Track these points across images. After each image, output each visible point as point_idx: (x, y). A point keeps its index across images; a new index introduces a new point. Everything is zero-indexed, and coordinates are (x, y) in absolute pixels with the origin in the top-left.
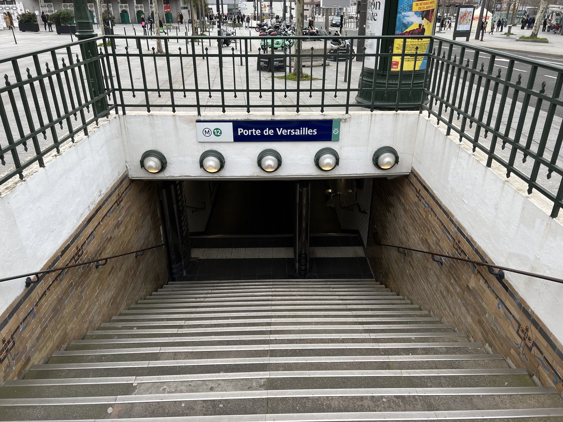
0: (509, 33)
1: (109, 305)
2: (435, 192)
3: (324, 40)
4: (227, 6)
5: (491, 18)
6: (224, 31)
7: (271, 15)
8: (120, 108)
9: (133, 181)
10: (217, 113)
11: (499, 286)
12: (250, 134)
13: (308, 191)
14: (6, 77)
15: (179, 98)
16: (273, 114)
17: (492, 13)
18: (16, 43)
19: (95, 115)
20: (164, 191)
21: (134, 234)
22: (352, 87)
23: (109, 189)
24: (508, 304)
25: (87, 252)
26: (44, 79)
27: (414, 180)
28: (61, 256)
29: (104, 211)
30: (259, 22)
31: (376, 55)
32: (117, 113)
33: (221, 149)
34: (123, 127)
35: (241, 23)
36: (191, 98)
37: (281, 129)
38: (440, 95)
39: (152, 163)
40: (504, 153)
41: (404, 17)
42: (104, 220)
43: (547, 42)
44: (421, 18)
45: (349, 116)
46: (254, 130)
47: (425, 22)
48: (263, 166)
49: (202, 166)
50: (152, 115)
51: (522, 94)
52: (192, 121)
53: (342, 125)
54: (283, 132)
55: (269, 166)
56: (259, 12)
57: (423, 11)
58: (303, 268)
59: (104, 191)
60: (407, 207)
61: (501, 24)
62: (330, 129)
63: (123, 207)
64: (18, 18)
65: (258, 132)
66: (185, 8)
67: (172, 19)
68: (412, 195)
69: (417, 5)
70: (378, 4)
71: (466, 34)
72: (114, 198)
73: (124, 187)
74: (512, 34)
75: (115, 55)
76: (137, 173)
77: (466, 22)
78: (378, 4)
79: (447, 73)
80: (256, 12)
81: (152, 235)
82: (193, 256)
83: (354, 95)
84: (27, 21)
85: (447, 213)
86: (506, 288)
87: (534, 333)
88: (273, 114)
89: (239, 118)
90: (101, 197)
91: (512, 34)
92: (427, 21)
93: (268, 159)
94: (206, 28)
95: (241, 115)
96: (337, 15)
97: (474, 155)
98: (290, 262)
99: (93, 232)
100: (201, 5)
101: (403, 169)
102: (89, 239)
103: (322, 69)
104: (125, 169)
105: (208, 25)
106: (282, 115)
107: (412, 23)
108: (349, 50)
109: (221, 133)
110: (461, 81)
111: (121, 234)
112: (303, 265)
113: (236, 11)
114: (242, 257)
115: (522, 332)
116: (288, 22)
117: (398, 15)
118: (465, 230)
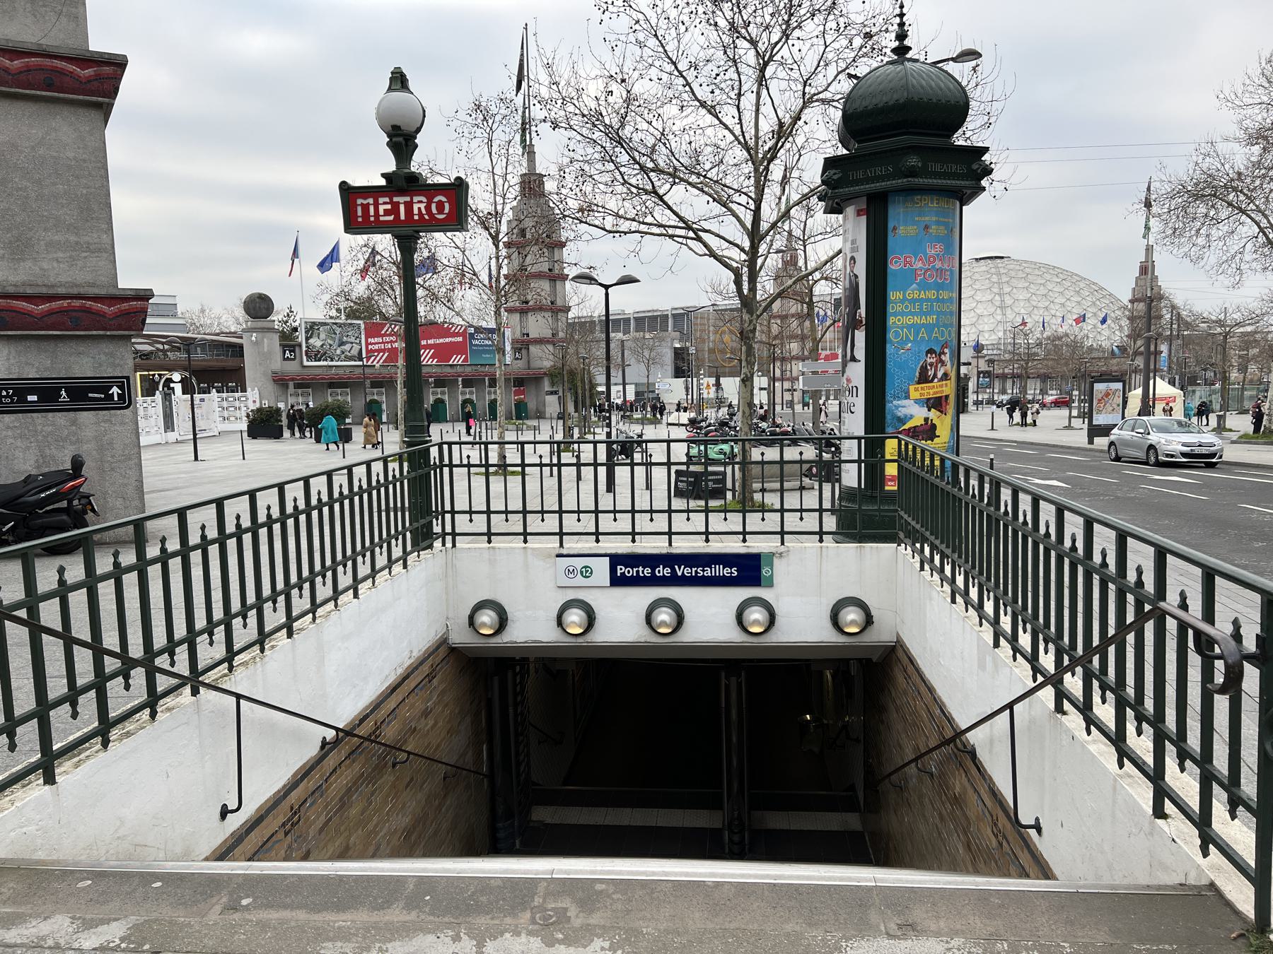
1: (400, 838)
2: (919, 662)
4: (633, 386)
5: (1180, 400)
6: (621, 432)
7: (720, 402)
8: (449, 538)
10: (587, 545)
11: (974, 771)
12: (635, 575)
13: (739, 685)
15: (570, 523)
16: (670, 544)
17: (1182, 390)
18: (244, 459)
20: (496, 679)
21: (444, 738)
23: (421, 653)
24: (982, 792)
25: (385, 735)
26: (40, 604)
27: (900, 653)
28: (359, 725)
29: (411, 683)
31: (859, 461)
32: (444, 544)
33: (591, 597)
34: (450, 565)
35: (658, 416)
36: (551, 523)
37: (683, 567)
39: (487, 618)
42: (411, 697)
44: (926, 409)
45: (786, 549)
46: (641, 569)
47: (933, 414)
48: (654, 625)
49: (560, 623)
50: (493, 548)
52: (549, 556)
53: (776, 561)
54: (685, 571)
55: (663, 624)
56: (695, 397)
57: (929, 399)
58: (736, 838)
59: (416, 654)
61: (1203, 410)
62: (758, 569)
63: (435, 687)
64: (248, 416)
65: (647, 572)
66: (551, 393)
67: (526, 413)
68: (900, 679)
69: (916, 390)
70: (855, 389)
72: (426, 669)
73: (438, 660)
74: (1230, 430)
75: (451, 466)
76: (461, 637)
77: (1111, 408)
78: (855, 389)
80: (690, 397)
81: (470, 754)
83: (830, 523)
84: (262, 421)
85: (931, 690)
88: (670, 544)
89: (620, 551)
90: (412, 661)
91: (1230, 430)
92: (938, 413)
93: (661, 612)
94: (589, 428)
95: (622, 546)
97: (943, 592)
98: (715, 834)
99: (395, 709)
100: (584, 390)
101: (881, 634)
102: (390, 718)
104: (445, 630)
105: (595, 422)
106: (683, 546)
107: (911, 417)
109: (591, 573)
111: (428, 731)
112: (736, 833)
113: (651, 396)
114: (626, 823)
117: (888, 406)
118: (945, 706)
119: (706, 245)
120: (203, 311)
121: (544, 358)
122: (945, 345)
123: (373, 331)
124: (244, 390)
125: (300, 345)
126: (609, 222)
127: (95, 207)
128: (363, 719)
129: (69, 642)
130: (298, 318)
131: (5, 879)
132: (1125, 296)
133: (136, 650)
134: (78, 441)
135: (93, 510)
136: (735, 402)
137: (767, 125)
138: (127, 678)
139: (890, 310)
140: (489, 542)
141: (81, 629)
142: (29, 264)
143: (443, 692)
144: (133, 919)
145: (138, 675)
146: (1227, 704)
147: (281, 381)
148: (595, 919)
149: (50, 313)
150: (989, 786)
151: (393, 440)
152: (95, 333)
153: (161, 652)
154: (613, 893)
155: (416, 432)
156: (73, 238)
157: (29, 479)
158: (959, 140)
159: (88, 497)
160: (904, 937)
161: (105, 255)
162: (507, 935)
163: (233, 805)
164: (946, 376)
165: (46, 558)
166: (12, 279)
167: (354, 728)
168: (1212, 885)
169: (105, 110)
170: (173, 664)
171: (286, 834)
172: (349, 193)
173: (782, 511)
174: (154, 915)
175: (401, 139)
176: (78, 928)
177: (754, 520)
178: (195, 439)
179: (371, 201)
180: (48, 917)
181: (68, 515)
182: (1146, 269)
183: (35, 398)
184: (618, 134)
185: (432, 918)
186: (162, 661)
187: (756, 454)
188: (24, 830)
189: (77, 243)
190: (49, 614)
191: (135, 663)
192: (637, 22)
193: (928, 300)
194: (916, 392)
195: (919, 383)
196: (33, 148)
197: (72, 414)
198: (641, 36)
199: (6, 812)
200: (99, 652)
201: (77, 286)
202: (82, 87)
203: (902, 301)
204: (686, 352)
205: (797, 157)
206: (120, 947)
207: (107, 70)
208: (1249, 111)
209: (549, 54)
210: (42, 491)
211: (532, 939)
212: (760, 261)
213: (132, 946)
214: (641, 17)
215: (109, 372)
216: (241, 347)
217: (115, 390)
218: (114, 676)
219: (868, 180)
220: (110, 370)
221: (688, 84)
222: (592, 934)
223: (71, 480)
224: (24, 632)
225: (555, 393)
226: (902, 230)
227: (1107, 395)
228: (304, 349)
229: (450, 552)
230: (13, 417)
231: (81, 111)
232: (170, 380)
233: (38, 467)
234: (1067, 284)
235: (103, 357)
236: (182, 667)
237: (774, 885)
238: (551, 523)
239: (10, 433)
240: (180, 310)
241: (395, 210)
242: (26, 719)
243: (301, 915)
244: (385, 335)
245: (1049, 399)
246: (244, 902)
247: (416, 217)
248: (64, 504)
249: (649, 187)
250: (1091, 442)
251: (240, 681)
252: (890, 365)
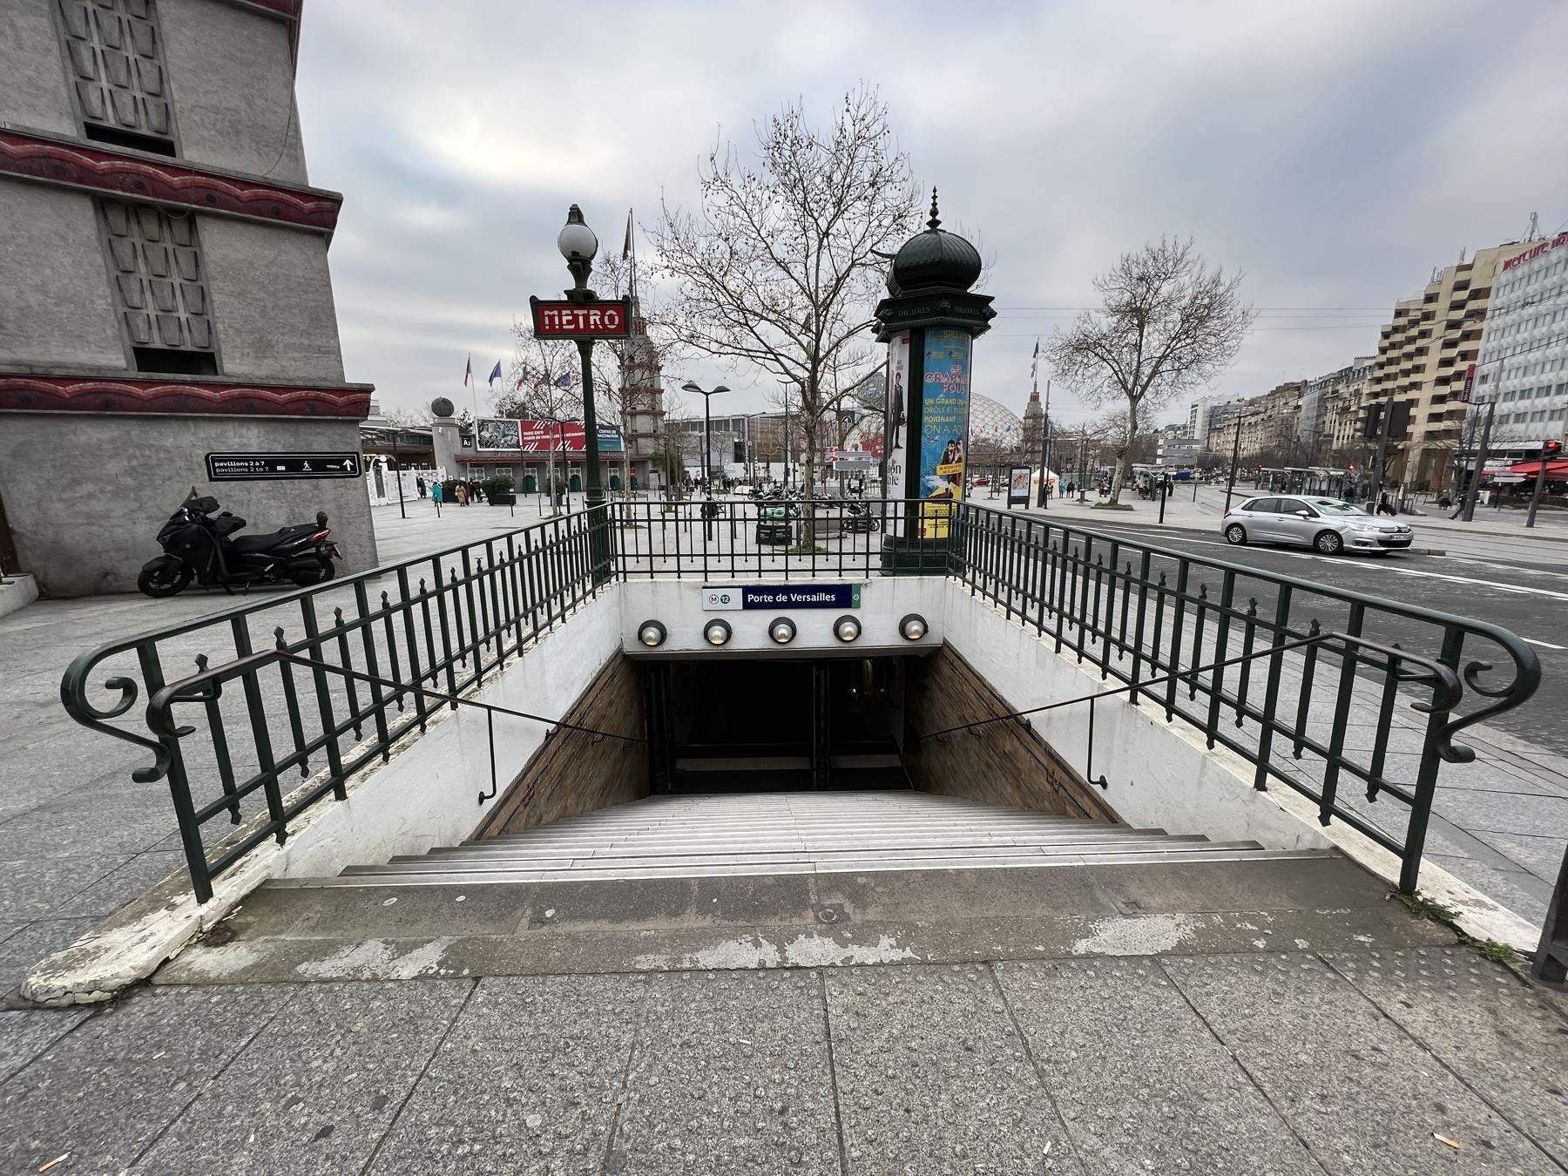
0: (1082, 499)
5: (1057, 481)
7: (768, 479)
8: (621, 575)
9: (625, 657)
10: (725, 579)
11: (1028, 738)
13: (826, 674)
15: (685, 563)
19: (593, 586)
24: (1037, 753)
27: (947, 652)
30: (752, 488)
36: (699, 563)
38: (994, 573)
39: (652, 633)
40: (1071, 634)
41: (928, 481)
43: (1132, 510)
47: (951, 486)
48: (775, 636)
51: (1080, 567)
55: (783, 636)
59: (603, 662)
60: (943, 685)
61: (1070, 488)
65: (770, 599)
66: (654, 472)
68: (946, 669)
71: (1025, 500)
72: (609, 671)
76: (632, 647)
82: (678, 767)
83: (876, 562)
85: (980, 679)
86: (1034, 738)
87: (1059, 774)
95: (752, 580)
96: (856, 479)
101: (934, 639)
103: (838, 541)
106: (796, 580)
107: (938, 487)
108: (868, 518)
110: (1016, 555)
115: (1050, 776)
116: (790, 486)
118: (996, 691)
119: (782, 365)
120: (399, 412)
121: (648, 447)
122: (959, 439)
123: (527, 427)
124: (434, 467)
125: (474, 436)
126: (714, 347)
127: (323, 317)
128: (572, 713)
129: (350, 676)
130: (471, 417)
131: (310, 902)
132: (1021, 416)
133: (406, 678)
134: (321, 502)
135: (337, 555)
137: (827, 276)
138: (400, 700)
139: (924, 412)
140: (652, 577)
141: (359, 664)
142: (270, 361)
143: (620, 689)
144: (446, 940)
145: (409, 697)
147: (461, 462)
148: (872, 914)
149: (291, 401)
150: (1045, 750)
151: (577, 502)
152: (329, 417)
153: (426, 677)
154: (876, 886)
155: (594, 495)
156: (306, 342)
157: (282, 531)
158: (972, 290)
159: (332, 545)
160: (1134, 916)
161: (333, 356)
162: (802, 937)
163: (488, 792)
164: (960, 460)
166: (257, 373)
167: (566, 721)
168: (1336, 849)
169: (326, 238)
170: (436, 686)
171: (525, 806)
172: (538, 306)
173: (840, 554)
174: (466, 934)
175: (579, 263)
176: (393, 955)
177: (821, 561)
178: (402, 502)
179: (556, 313)
180: (360, 944)
181: (318, 558)
182: (1035, 398)
183: (283, 468)
185: (726, 922)
186: (427, 685)
187: (820, 514)
188: (321, 844)
189: (310, 346)
190: (330, 652)
191: (405, 689)
192: (732, 198)
193: (949, 405)
194: (942, 470)
195: (943, 464)
196: (267, 266)
197: (314, 481)
198: (736, 209)
199: (304, 831)
200: (375, 681)
201: (311, 380)
202: (306, 217)
203: (933, 406)
205: (840, 306)
206: (439, 974)
207: (326, 204)
208: (1112, 294)
209: (672, 215)
210: (295, 541)
211: (826, 940)
212: (819, 375)
213: (452, 972)
214: (734, 195)
215: (343, 449)
216: (431, 437)
217: (348, 463)
218: (390, 700)
219: (908, 318)
220: (342, 447)
221: (768, 247)
222: (877, 931)
223: (317, 532)
224: (309, 671)
225: (656, 472)
226: (934, 354)
227: (1020, 477)
228: (478, 439)
229: (622, 585)
230: (266, 482)
231: (306, 238)
232: (378, 461)
233: (290, 522)
234: (986, 406)
235: (337, 437)
236: (443, 689)
237: (1005, 869)
238: (672, 563)
239: (264, 495)
240: (381, 411)
241: (575, 321)
242: (316, 746)
243: (605, 926)
244: (536, 430)
245: (975, 480)
246: (549, 914)
247: (592, 327)
248: (313, 550)
249: (742, 321)
250: (1009, 507)
251: (487, 695)
252: (924, 451)
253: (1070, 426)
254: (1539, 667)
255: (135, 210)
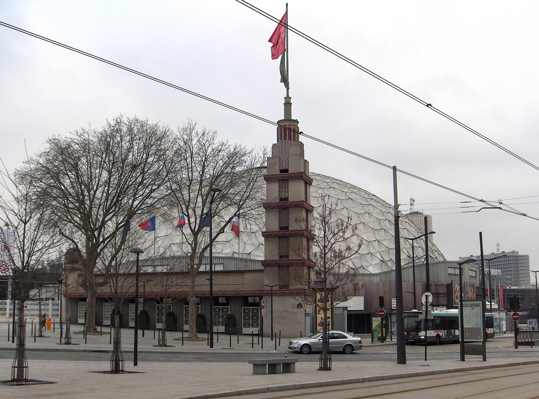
3: (393, 308)
14: (143, 336)
22: (216, 279)
53: (252, 372)
79: (385, 279)
103: (102, 331)
136: (313, 246)
146: (220, 270)
165: (452, 345)
184: (216, 215)
204: (266, 176)
253: (28, 162)
254: (96, 301)
255: (283, 180)
